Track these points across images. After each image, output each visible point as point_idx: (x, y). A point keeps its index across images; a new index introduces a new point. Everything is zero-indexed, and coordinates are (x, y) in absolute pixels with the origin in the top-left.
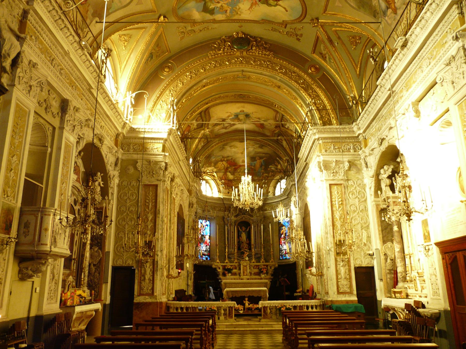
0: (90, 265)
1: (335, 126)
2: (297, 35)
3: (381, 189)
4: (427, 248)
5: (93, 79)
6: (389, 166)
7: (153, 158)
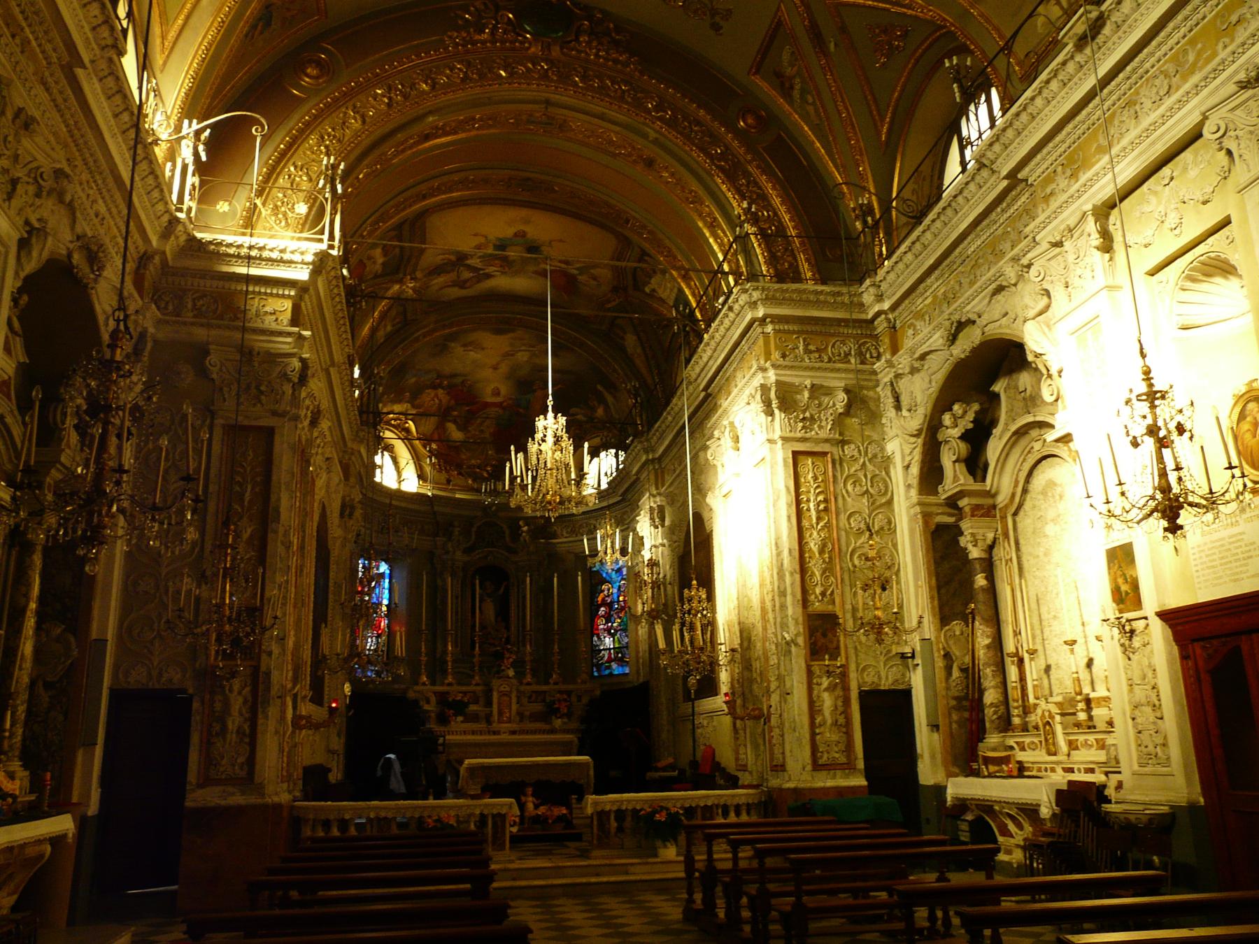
0: (33, 684)
1: (810, 286)
2: (714, 12)
3: (940, 471)
4: (1128, 628)
5: (87, 29)
6: (968, 404)
7: (260, 342)
